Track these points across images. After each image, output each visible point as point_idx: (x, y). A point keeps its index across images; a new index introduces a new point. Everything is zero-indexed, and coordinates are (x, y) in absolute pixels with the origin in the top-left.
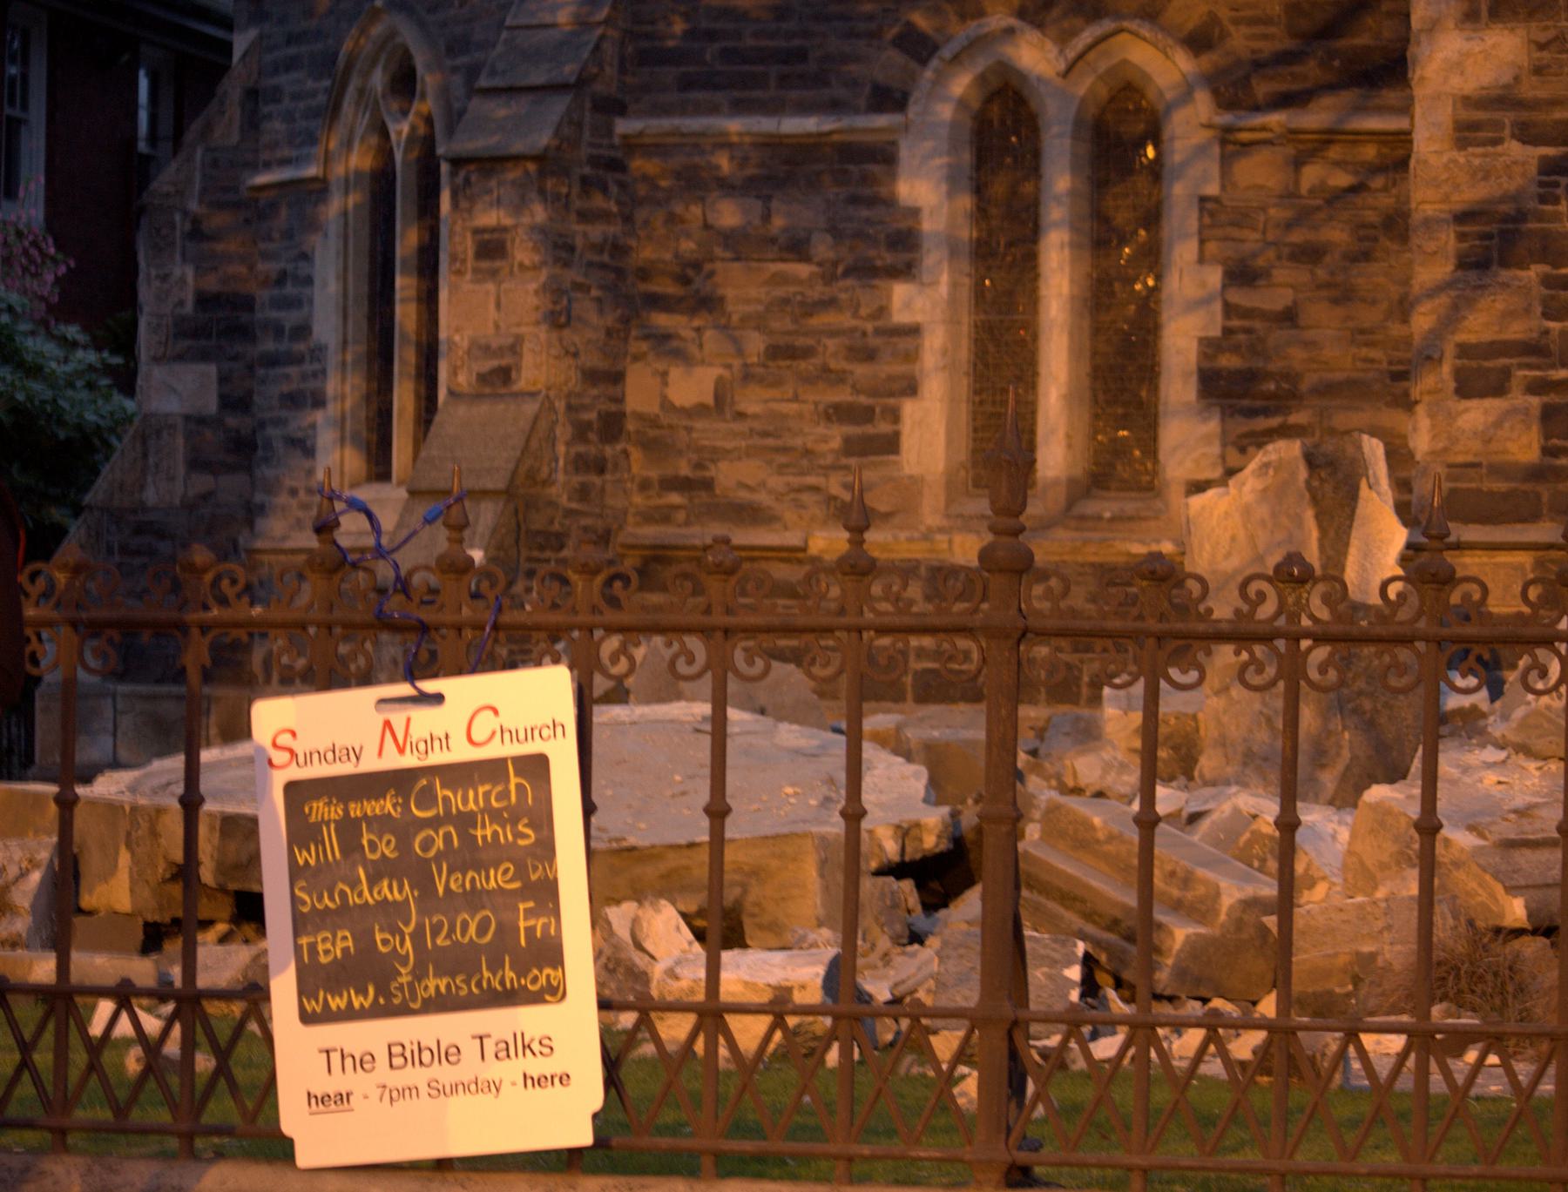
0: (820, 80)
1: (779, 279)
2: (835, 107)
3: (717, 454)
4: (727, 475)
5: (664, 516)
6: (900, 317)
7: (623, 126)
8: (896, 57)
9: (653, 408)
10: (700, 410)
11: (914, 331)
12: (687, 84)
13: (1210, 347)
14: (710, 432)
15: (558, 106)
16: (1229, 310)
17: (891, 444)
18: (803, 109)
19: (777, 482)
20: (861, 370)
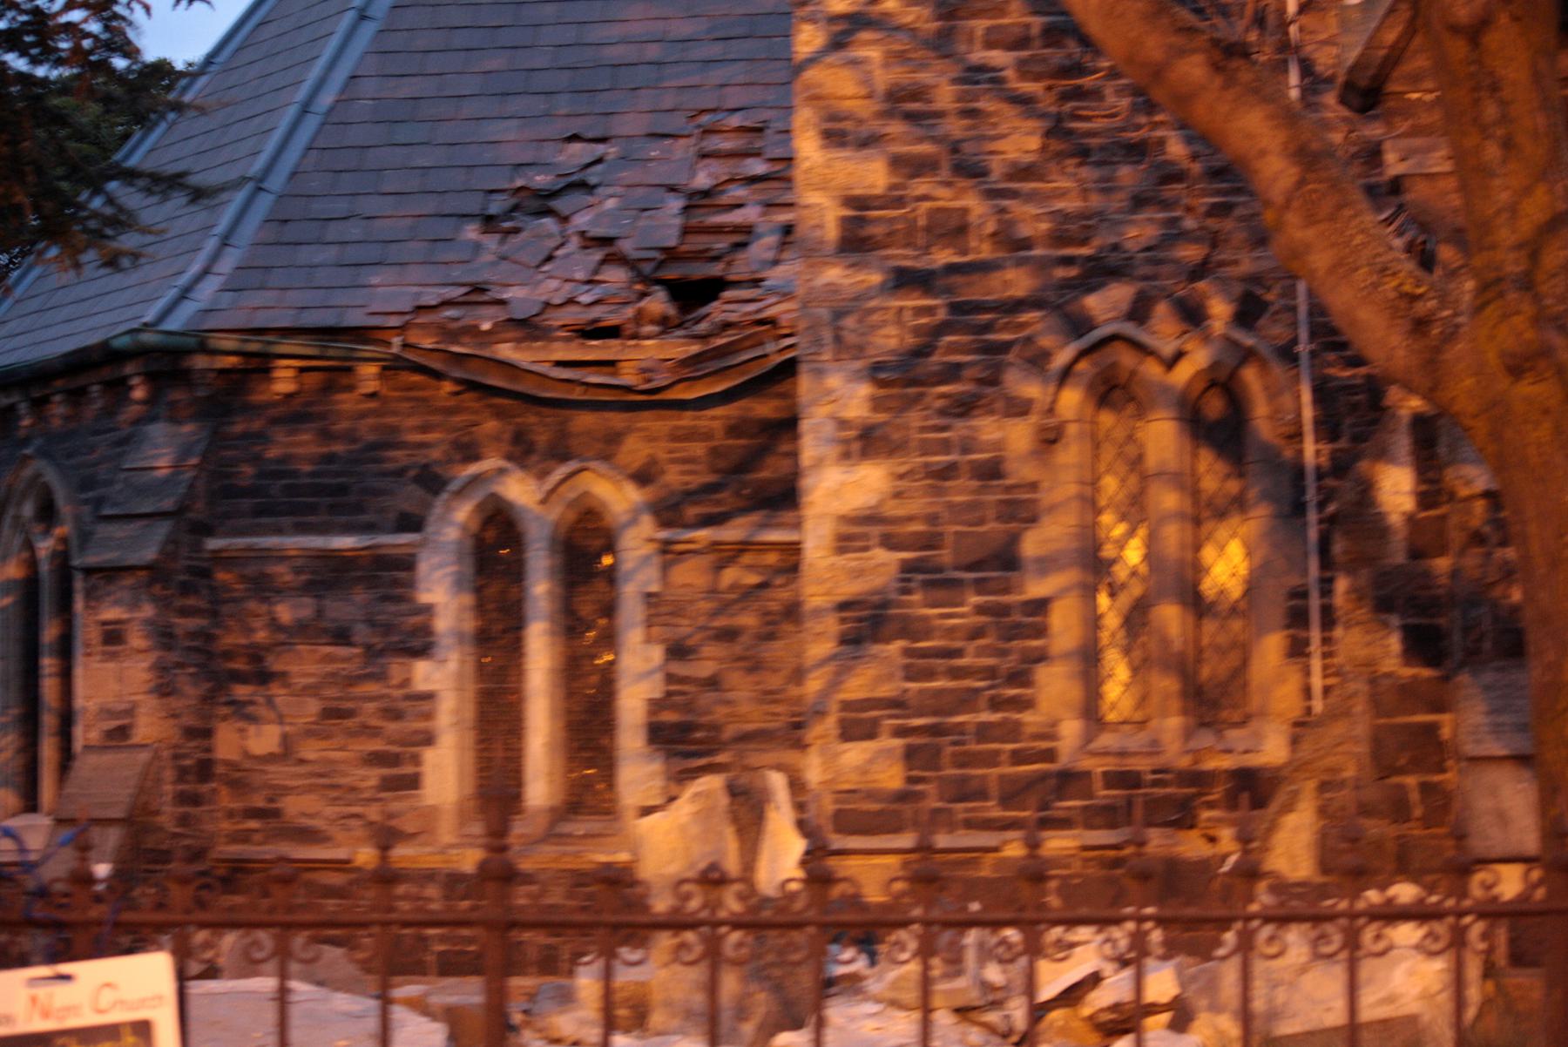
0: (359, 508)
1: (330, 659)
2: (369, 528)
3: (287, 790)
4: (293, 806)
5: (244, 837)
6: (421, 686)
7: (213, 544)
8: (416, 491)
9: (234, 756)
10: (271, 758)
11: (429, 696)
12: (259, 512)
13: (655, 706)
14: (280, 774)
15: (162, 529)
16: (670, 678)
17: (413, 782)
18: (348, 529)
19: (330, 811)
20: (392, 727)
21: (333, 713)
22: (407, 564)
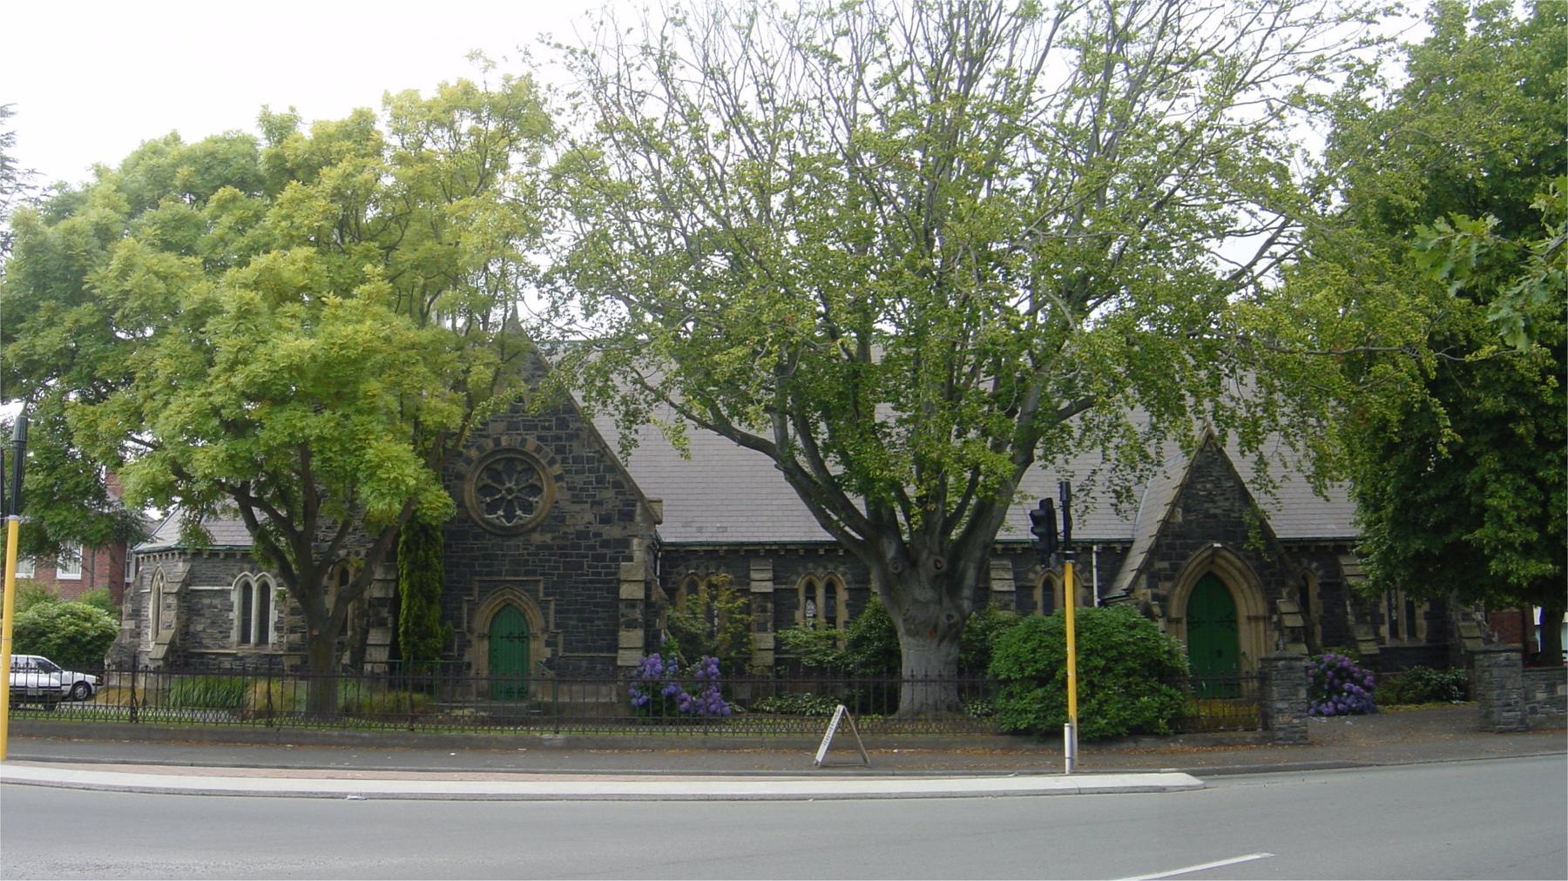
14: (202, 635)
21: (213, 623)
22: (229, 592)
